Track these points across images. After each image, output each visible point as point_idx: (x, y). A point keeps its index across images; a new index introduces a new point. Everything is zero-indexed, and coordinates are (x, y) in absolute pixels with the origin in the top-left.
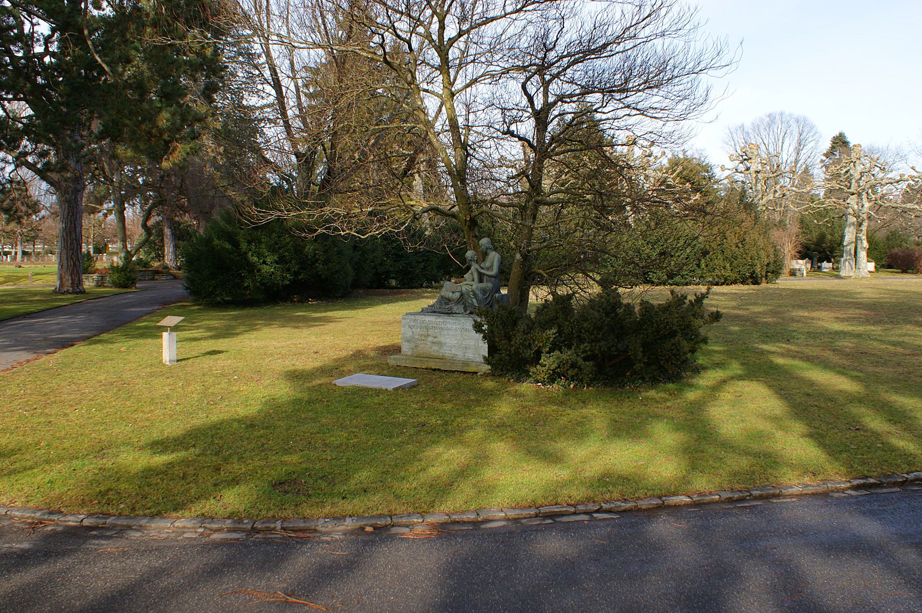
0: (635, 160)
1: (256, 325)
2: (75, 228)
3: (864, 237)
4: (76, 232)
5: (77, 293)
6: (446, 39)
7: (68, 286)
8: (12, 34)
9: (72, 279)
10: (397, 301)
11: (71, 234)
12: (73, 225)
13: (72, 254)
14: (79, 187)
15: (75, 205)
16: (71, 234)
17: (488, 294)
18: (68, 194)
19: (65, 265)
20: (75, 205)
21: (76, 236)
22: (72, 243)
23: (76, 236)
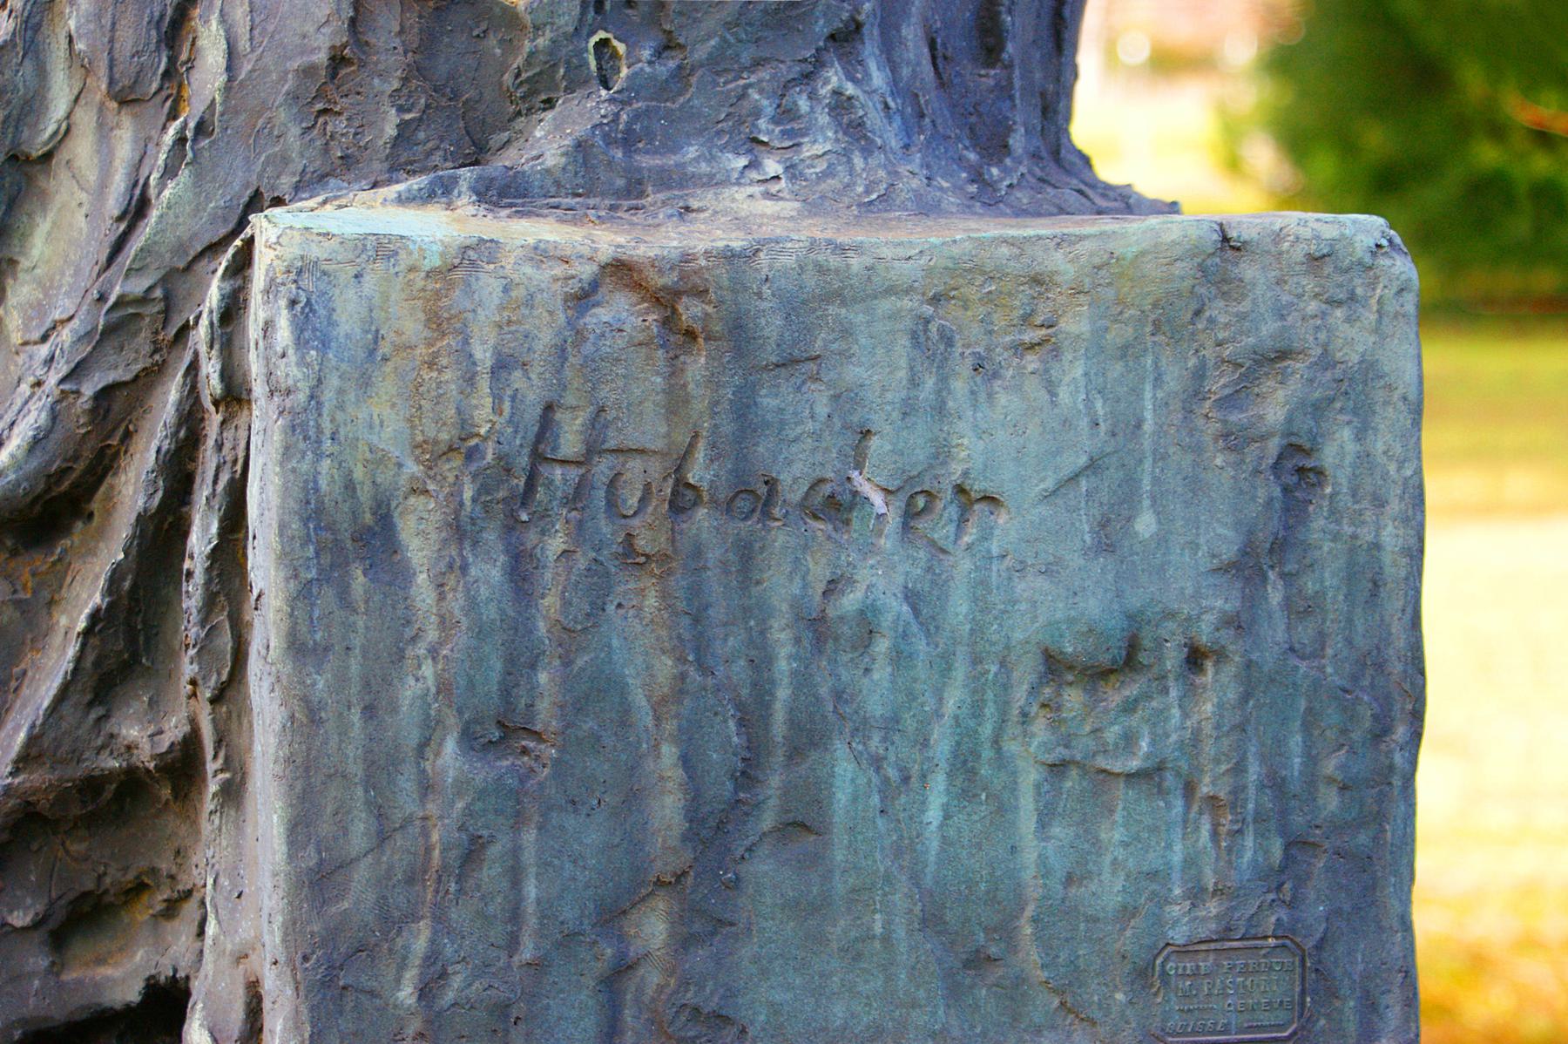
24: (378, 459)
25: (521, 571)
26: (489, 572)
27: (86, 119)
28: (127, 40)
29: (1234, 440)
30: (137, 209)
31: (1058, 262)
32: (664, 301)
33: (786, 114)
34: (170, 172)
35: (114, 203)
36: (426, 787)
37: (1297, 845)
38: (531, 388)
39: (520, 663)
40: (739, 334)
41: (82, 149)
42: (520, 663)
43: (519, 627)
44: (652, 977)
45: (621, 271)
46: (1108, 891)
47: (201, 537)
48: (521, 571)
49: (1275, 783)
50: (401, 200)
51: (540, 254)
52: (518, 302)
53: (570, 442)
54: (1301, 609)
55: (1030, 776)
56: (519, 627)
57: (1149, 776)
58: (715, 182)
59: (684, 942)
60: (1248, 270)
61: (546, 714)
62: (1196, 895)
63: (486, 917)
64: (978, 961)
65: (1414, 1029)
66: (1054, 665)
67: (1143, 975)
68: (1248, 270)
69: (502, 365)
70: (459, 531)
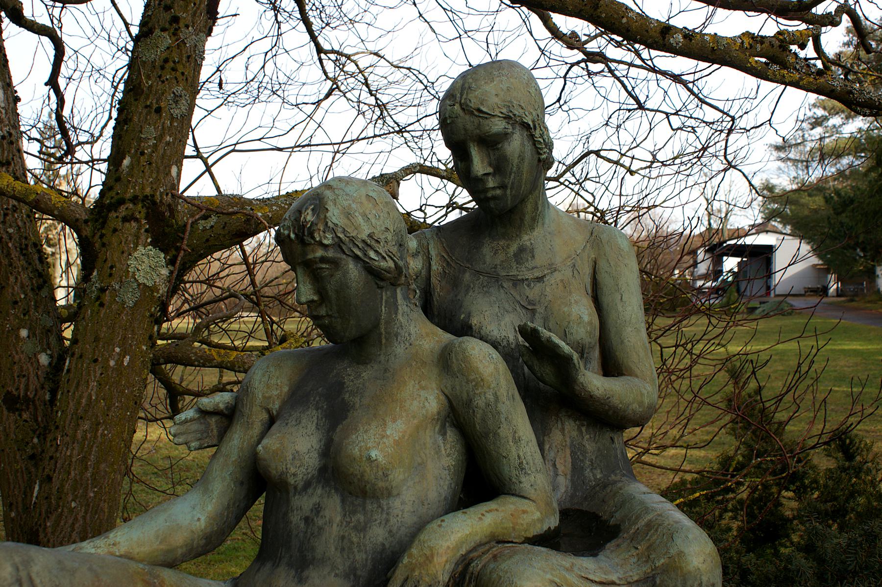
10: (795, 274)
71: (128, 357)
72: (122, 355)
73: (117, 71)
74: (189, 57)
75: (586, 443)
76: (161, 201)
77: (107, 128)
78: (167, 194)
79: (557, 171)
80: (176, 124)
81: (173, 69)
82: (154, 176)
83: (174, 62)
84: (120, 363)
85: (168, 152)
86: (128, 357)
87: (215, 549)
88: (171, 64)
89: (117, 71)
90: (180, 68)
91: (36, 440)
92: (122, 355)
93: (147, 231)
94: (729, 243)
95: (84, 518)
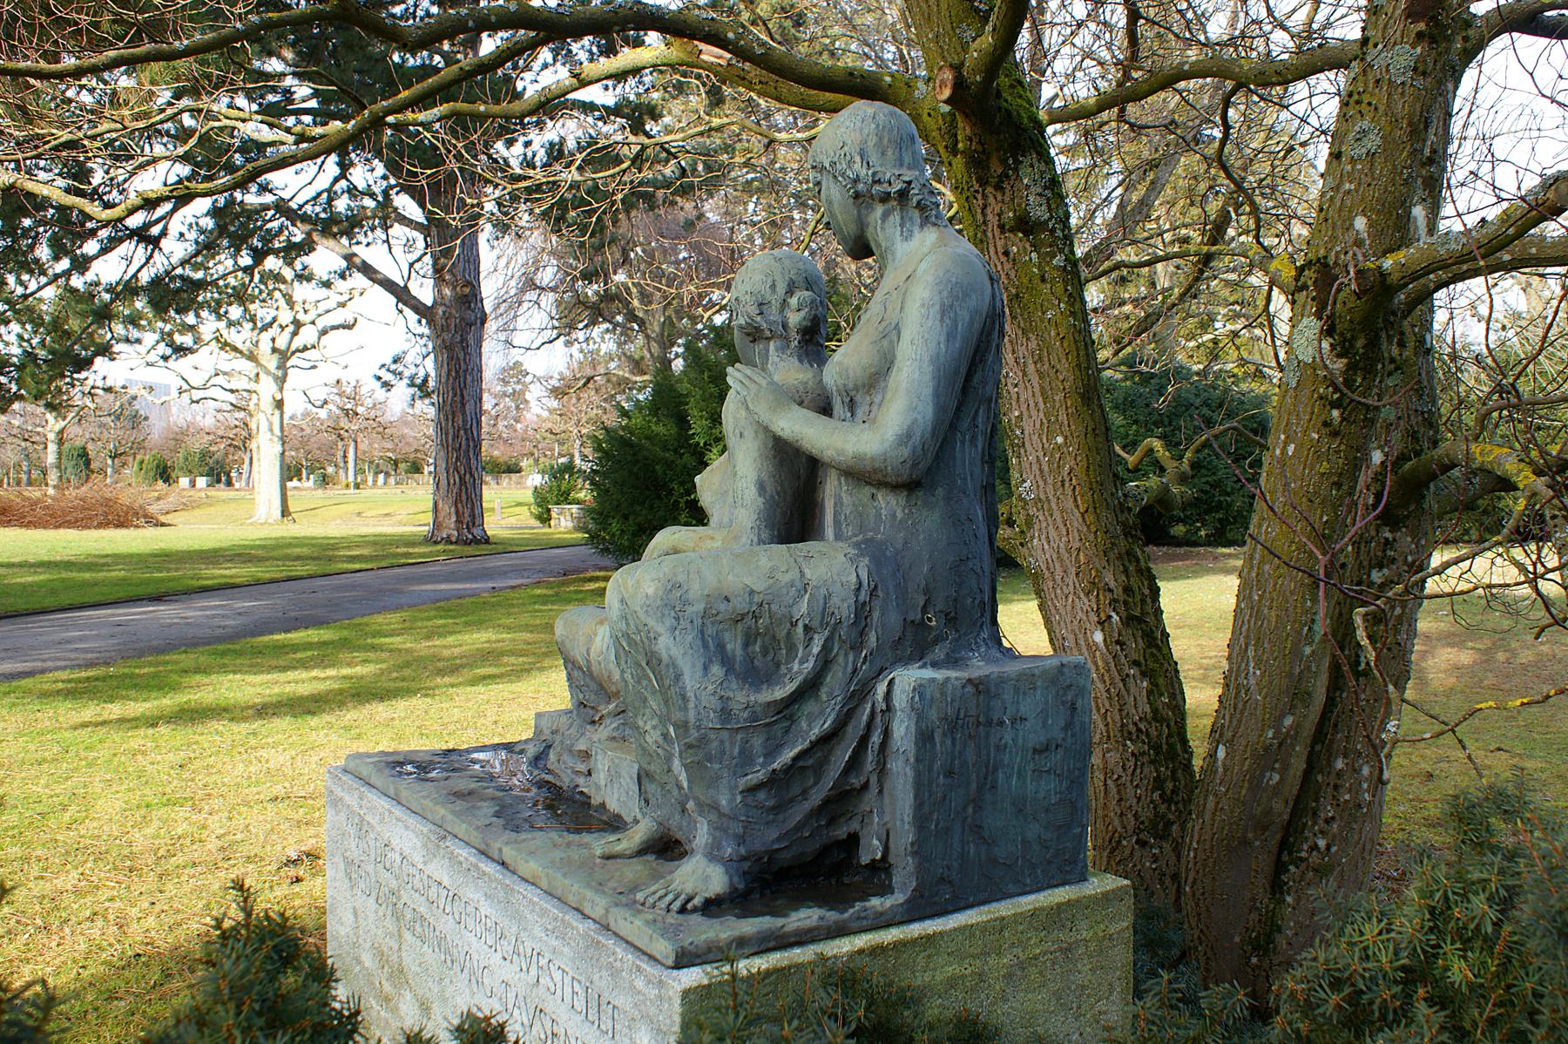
0: (885, 216)
1: (437, 687)
2: (463, 405)
3: (692, 731)
4: (464, 413)
5: (467, 543)
6: (269, 176)
7: (450, 528)
8: (396, 58)
9: (457, 512)
10: (1196, 574)
11: (454, 414)
12: (458, 398)
13: (458, 459)
14: (470, 316)
15: (461, 355)
16: (454, 414)
17: (801, 668)
18: (449, 331)
19: (444, 482)
20: (461, 355)
21: (465, 421)
22: (456, 436)
23: (465, 421)
24: (933, 722)
25: (954, 739)
26: (949, 742)
27: (842, 652)
28: (853, 636)
29: (1063, 703)
30: (855, 671)
31: (1036, 671)
32: (976, 686)
33: (976, 643)
34: (864, 663)
35: (850, 669)
36: (938, 786)
37: (1072, 782)
38: (956, 705)
39: (953, 761)
40: (988, 691)
41: (841, 659)
42: (953, 761)
43: (953, 752)
44: (969, 819)
45: (969, 680)
46: (1042, 794)
47: (876, 739)
48: (954, 739)
49: (1069, 769)
50: (920, 668)
51: (957, 679)
52: (954, 688)
53: (962, 716)
54: (1073, 735)
55: (1030, 773)
56: (953, 752)
57: (1048, 772)
58: (970, 659)
59: (975, 812)
60: (1065, 670)
61: (956, 770)
62: (1056, 793)
63: (1460, 858)
64: (1021, 810)
65: (481, 756)
66: (1035, 750)
67: (1047, 811)
68: (1065, 670)
69: (952, 701)
70: (944, 734)
71: (1293, 446)
72: (1286, 444)
73: (1543, 96)
74: (1378, 81)
75: (843, 495)
76: (1335, 263)
77: (139, 265)
78: (1346, 253)
79: (271, 430)
80: (1359, 167)
81: (1358, 102)
82: (1330, 233)
83: (1359, 93)
84: (1284, 450)
85: (1348, 203)
86: (1293, 446)
87: (1295, 804)
88: (1356, 97)
89: (1543, 96)
90: (1366, 98)
91: (1350, 548)
92: (1286, 444)
93: (1313, 299)
94: (551, 592)
95: (1249, 621)
